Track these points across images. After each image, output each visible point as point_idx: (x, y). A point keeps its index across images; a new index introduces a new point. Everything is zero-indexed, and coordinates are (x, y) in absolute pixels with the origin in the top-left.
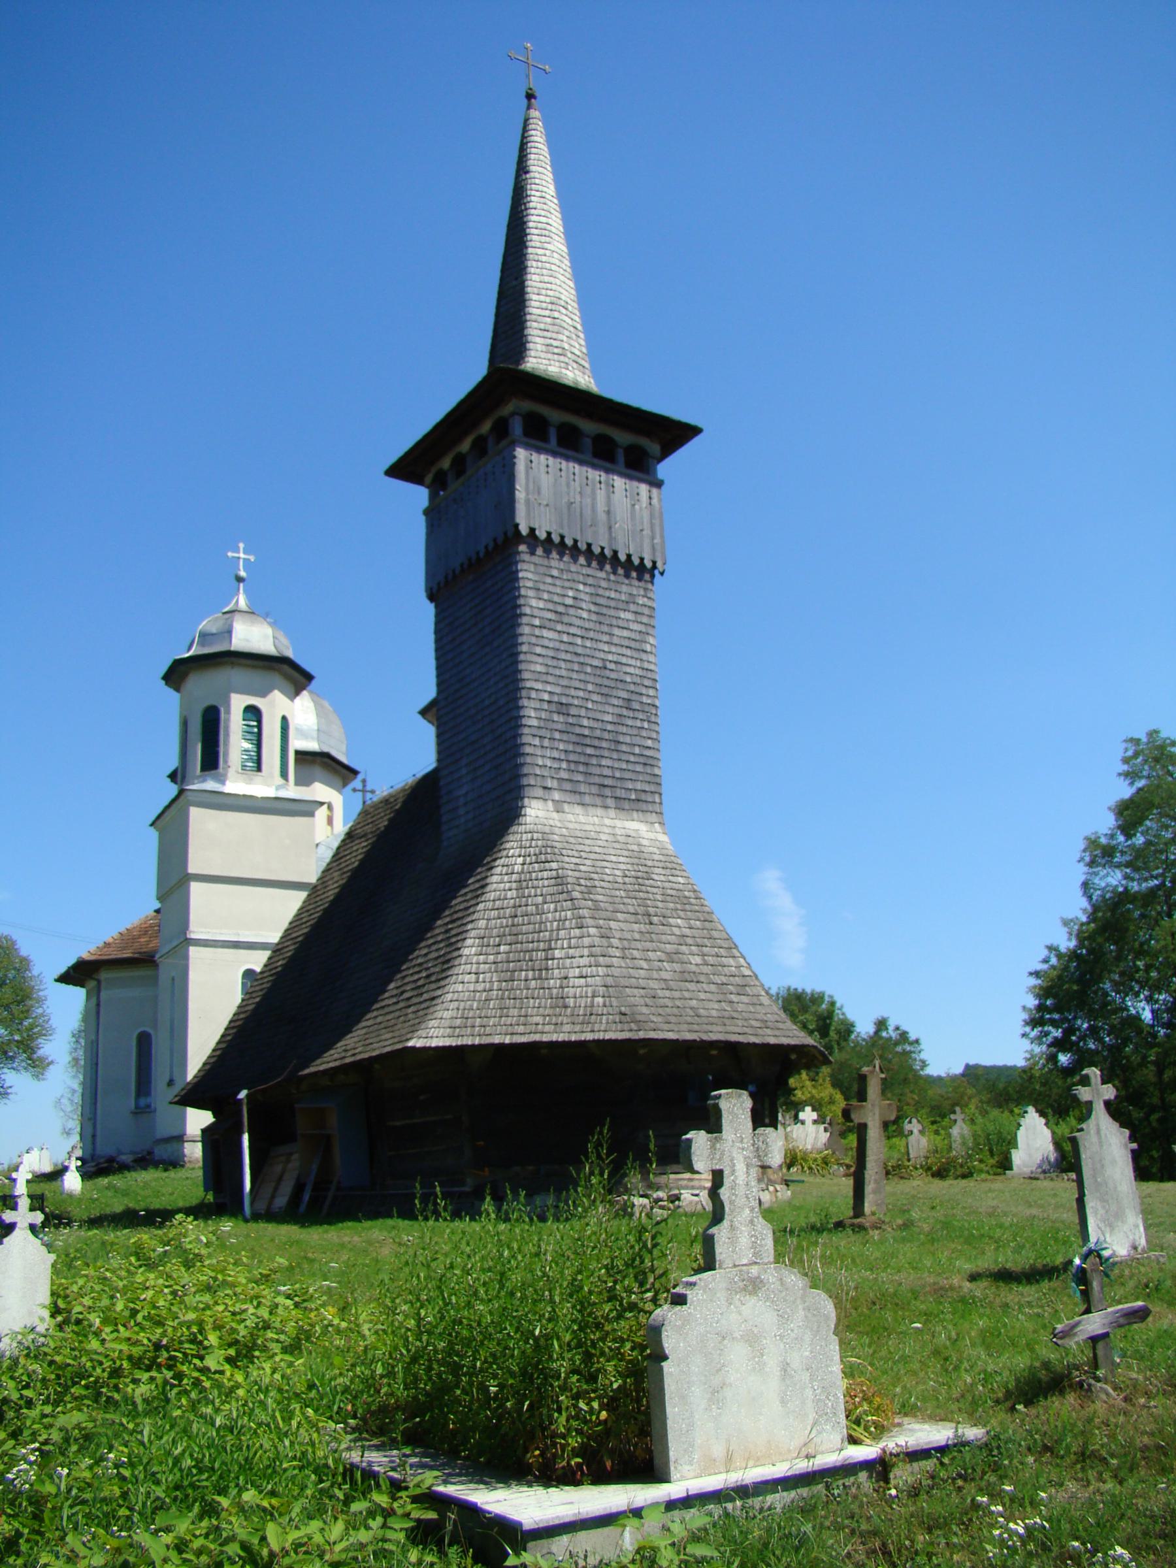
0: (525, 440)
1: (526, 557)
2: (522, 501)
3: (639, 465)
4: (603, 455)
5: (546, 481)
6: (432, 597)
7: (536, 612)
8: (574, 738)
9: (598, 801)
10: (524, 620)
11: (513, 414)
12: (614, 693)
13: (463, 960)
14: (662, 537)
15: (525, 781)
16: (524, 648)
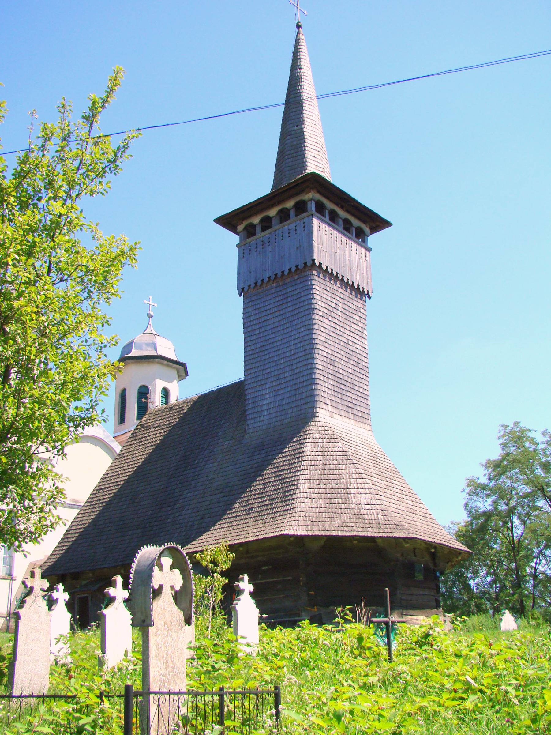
0: (317, 214)
1: (316, 278)
2: (316, 247)
3: (360, 236)
4: (347, 228)
5: (325, 238)
6: (242, 291)
7: (321, 309)
8: (336, 379)
9: (346, 414)
10: (316, 311)
11: (311, 200)
12: (352, 358)
13: (302, 491)
14: (371, 279)
15: (317, 398)
16: (316, 327)
